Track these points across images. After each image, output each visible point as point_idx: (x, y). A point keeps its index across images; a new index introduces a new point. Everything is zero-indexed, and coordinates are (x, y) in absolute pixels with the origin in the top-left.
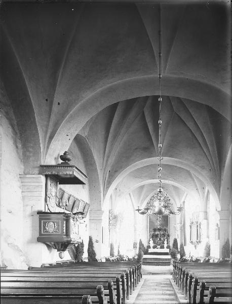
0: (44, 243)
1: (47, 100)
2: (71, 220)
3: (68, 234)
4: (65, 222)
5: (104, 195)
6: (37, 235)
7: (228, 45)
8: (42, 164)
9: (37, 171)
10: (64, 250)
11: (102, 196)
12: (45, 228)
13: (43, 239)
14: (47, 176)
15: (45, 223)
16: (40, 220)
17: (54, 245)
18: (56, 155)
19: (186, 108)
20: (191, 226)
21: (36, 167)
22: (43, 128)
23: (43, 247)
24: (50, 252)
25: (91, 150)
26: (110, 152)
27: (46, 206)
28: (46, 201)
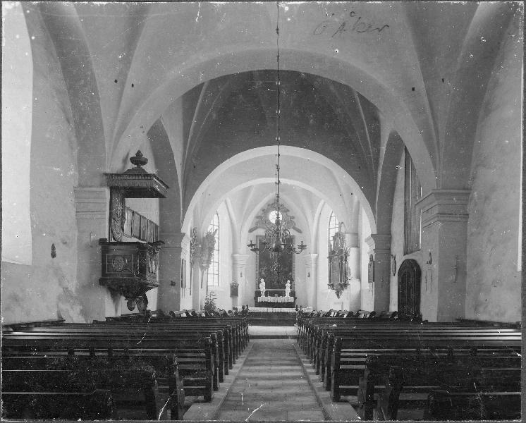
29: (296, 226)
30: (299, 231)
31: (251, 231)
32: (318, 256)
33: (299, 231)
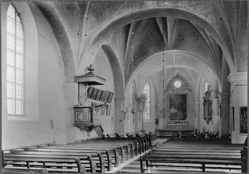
0: (78, 127)
1: (78, 34)
2: (94, 111)
3: (92, 121)
4: (90, 113)
5: (126, 82)
6: (74, 122)
7: (130, 89)
8: (77, 75)
9: (73, 80)
10: (90, 131)
11: (124, 85)
12: (78, 117)
13: (78, 124)
14: (79, 83)
15: (78, 114)
16: (75, 112)
17: (84, 128)
18: (85, 67)
19: (191, 23)
20: (204, 104)
21: (73, 77)
22: (57, 28)
23: (77, 130)
24: (83, 132)
25: (113, 52)
26: (131, 42)
27: (79, 102)
28: (79, 99)
29: (189, 88)
30: (191, 91)
31: (165, 92)
32: (200, 103)
33: (191, 91)
